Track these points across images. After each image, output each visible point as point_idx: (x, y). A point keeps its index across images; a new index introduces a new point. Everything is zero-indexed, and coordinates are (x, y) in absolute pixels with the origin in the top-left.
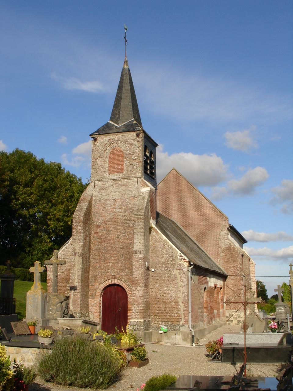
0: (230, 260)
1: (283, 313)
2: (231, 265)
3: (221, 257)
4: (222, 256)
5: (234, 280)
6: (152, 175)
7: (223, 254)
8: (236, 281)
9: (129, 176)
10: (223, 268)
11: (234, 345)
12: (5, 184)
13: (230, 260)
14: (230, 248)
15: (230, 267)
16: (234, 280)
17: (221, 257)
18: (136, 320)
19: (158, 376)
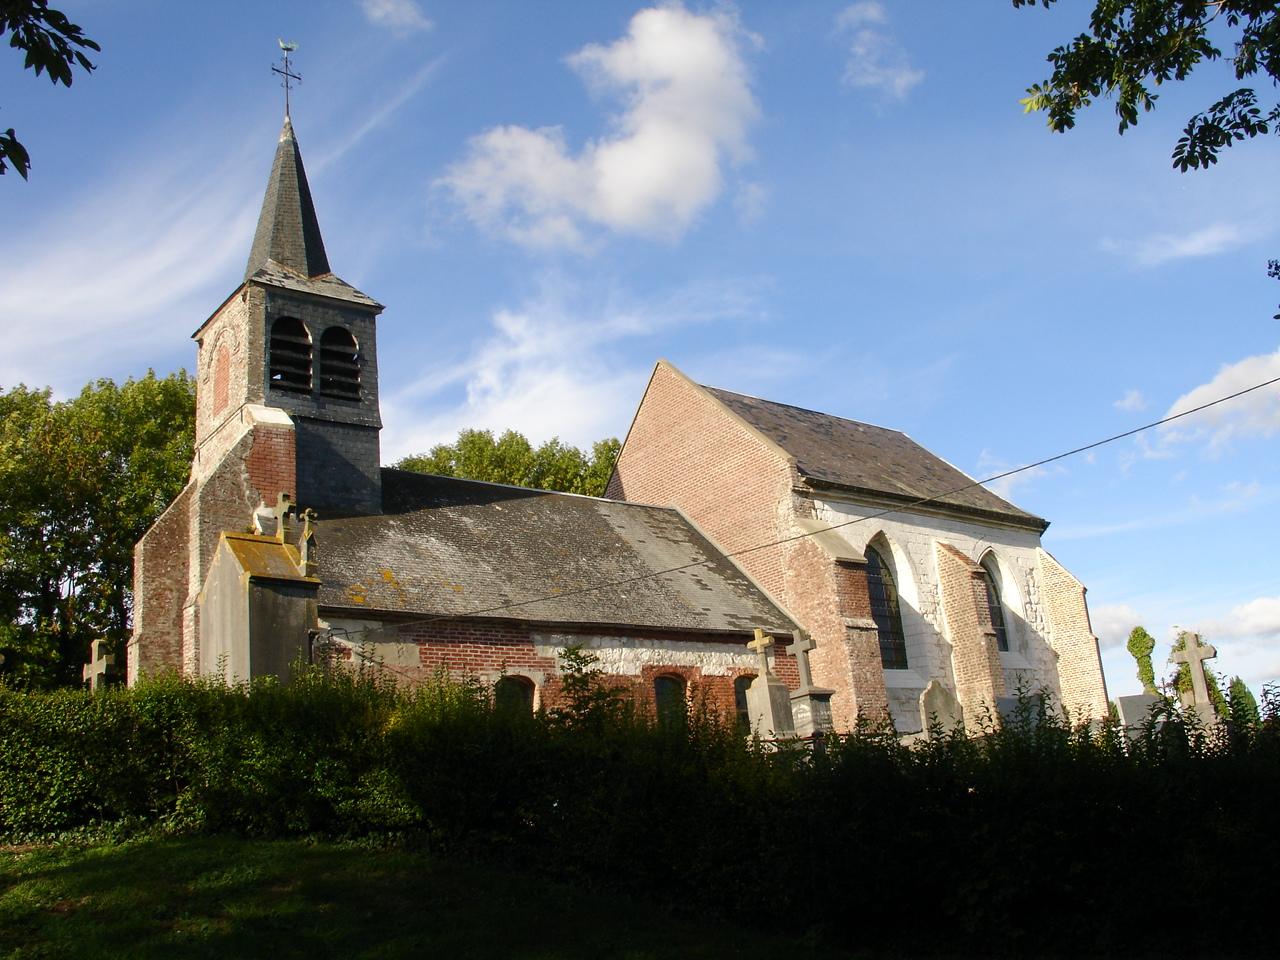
0: (809, 585)
1: (809, 723)
2: (813, 599)
3: (787, 582)
4: (788, 578)
5: (825, 645)
6: (256, 486)
7: (791, 573)
8: (832, 649)
9: (249, 504)
10: (795, 614)
11: (224, 646)
12: (99, 564)
13: (809, 585)
14: (805, 548)
15: (812, 608)
16: (825, 645)
17: (787, 582)
18: (923, 717)
19: (413, 689)
